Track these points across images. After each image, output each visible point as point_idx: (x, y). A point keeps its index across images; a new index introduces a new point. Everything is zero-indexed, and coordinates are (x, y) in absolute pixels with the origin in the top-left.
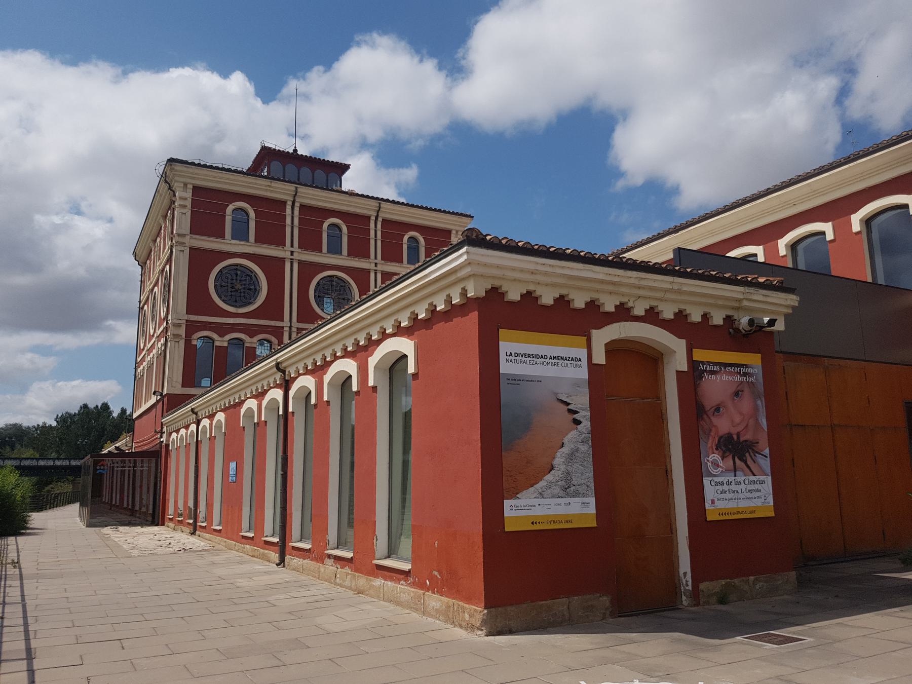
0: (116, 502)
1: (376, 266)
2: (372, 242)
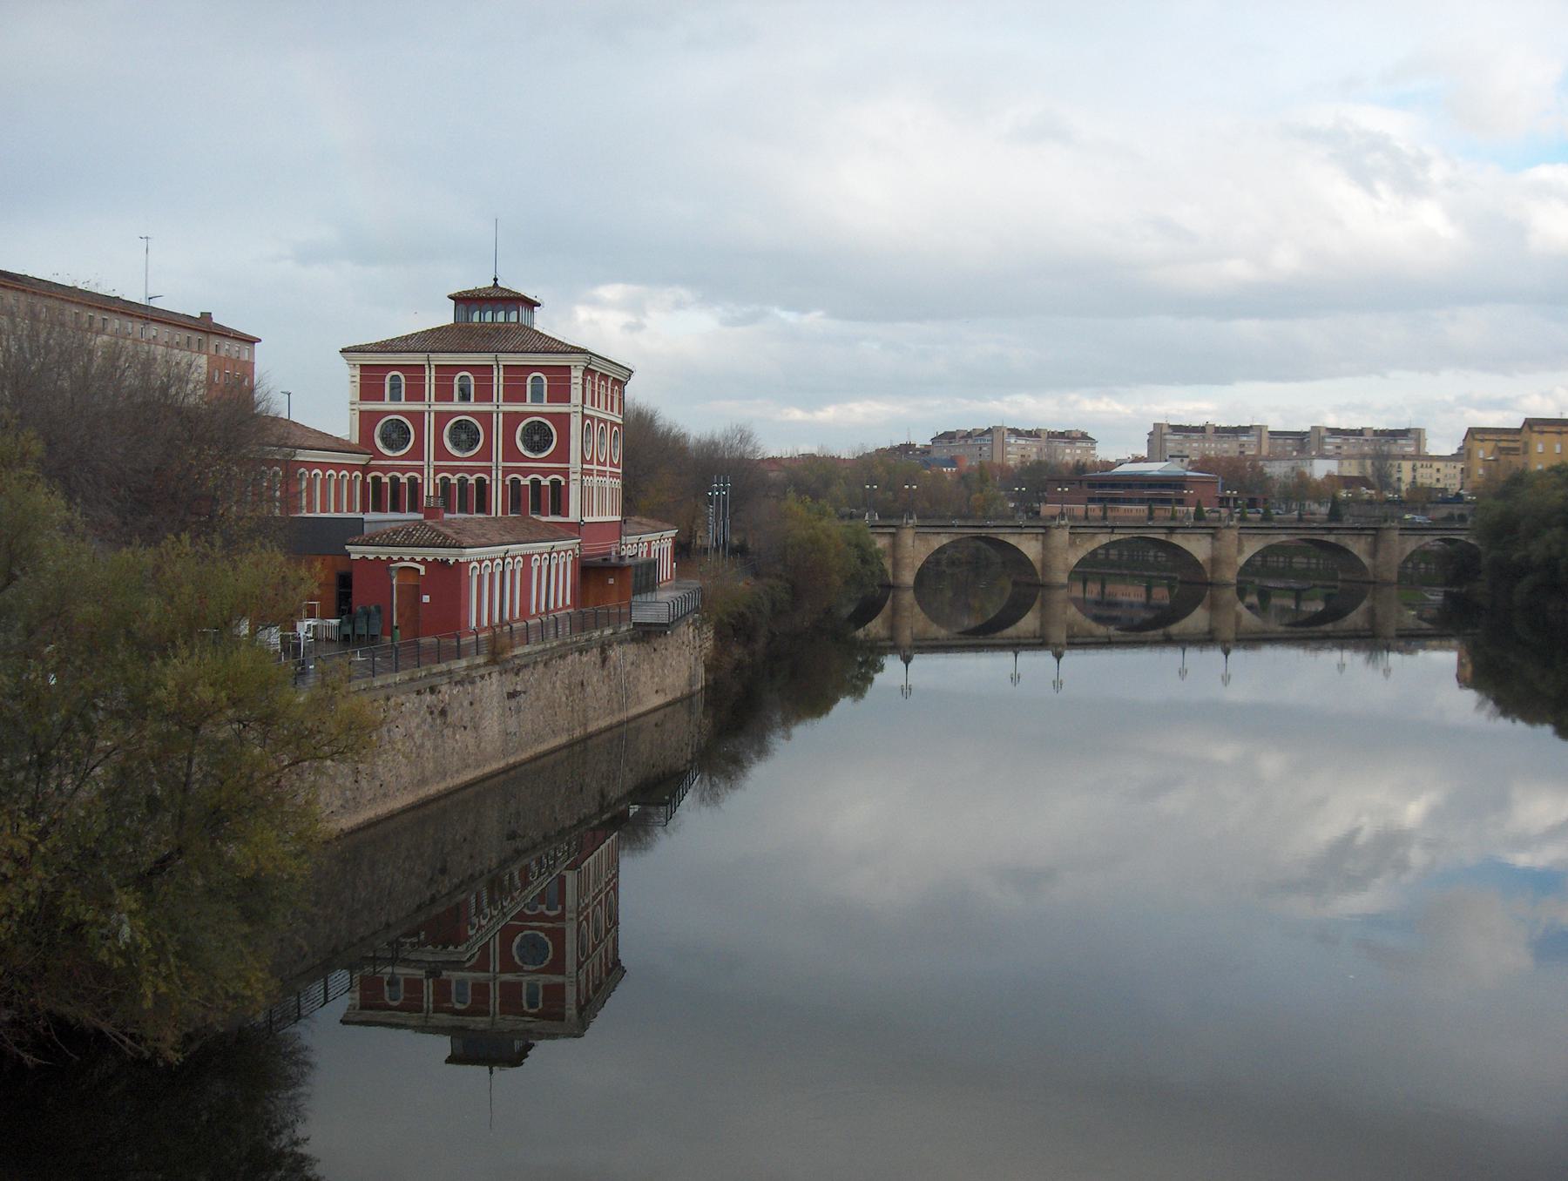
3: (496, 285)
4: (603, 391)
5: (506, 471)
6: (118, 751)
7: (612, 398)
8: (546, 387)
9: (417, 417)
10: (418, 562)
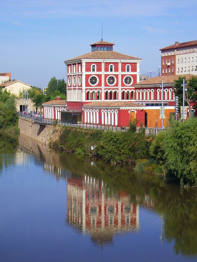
2: (102, 68)
9: (100, 76)
10: (135, 110)
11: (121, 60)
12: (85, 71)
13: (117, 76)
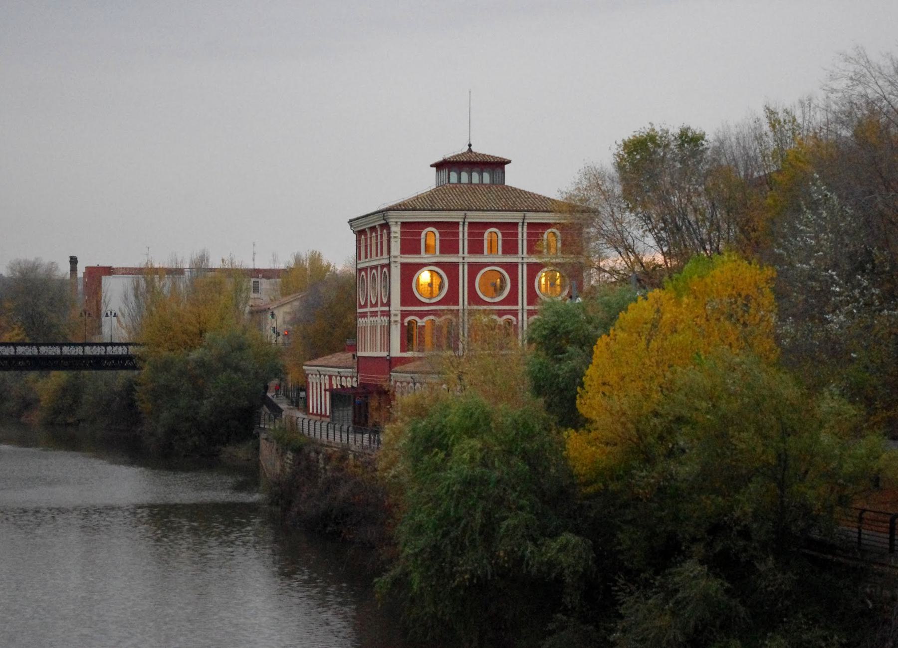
0: (313, 411)
1: (463, 259)
2: (520, 242)
3: (470, 150)
4: (374, 241)
5: (471, 313)
6: (444, 491)
7: (382, 243)
8: (500, 243)
11: (469, 213)
12: (401, 249)
13: (512, 268)
